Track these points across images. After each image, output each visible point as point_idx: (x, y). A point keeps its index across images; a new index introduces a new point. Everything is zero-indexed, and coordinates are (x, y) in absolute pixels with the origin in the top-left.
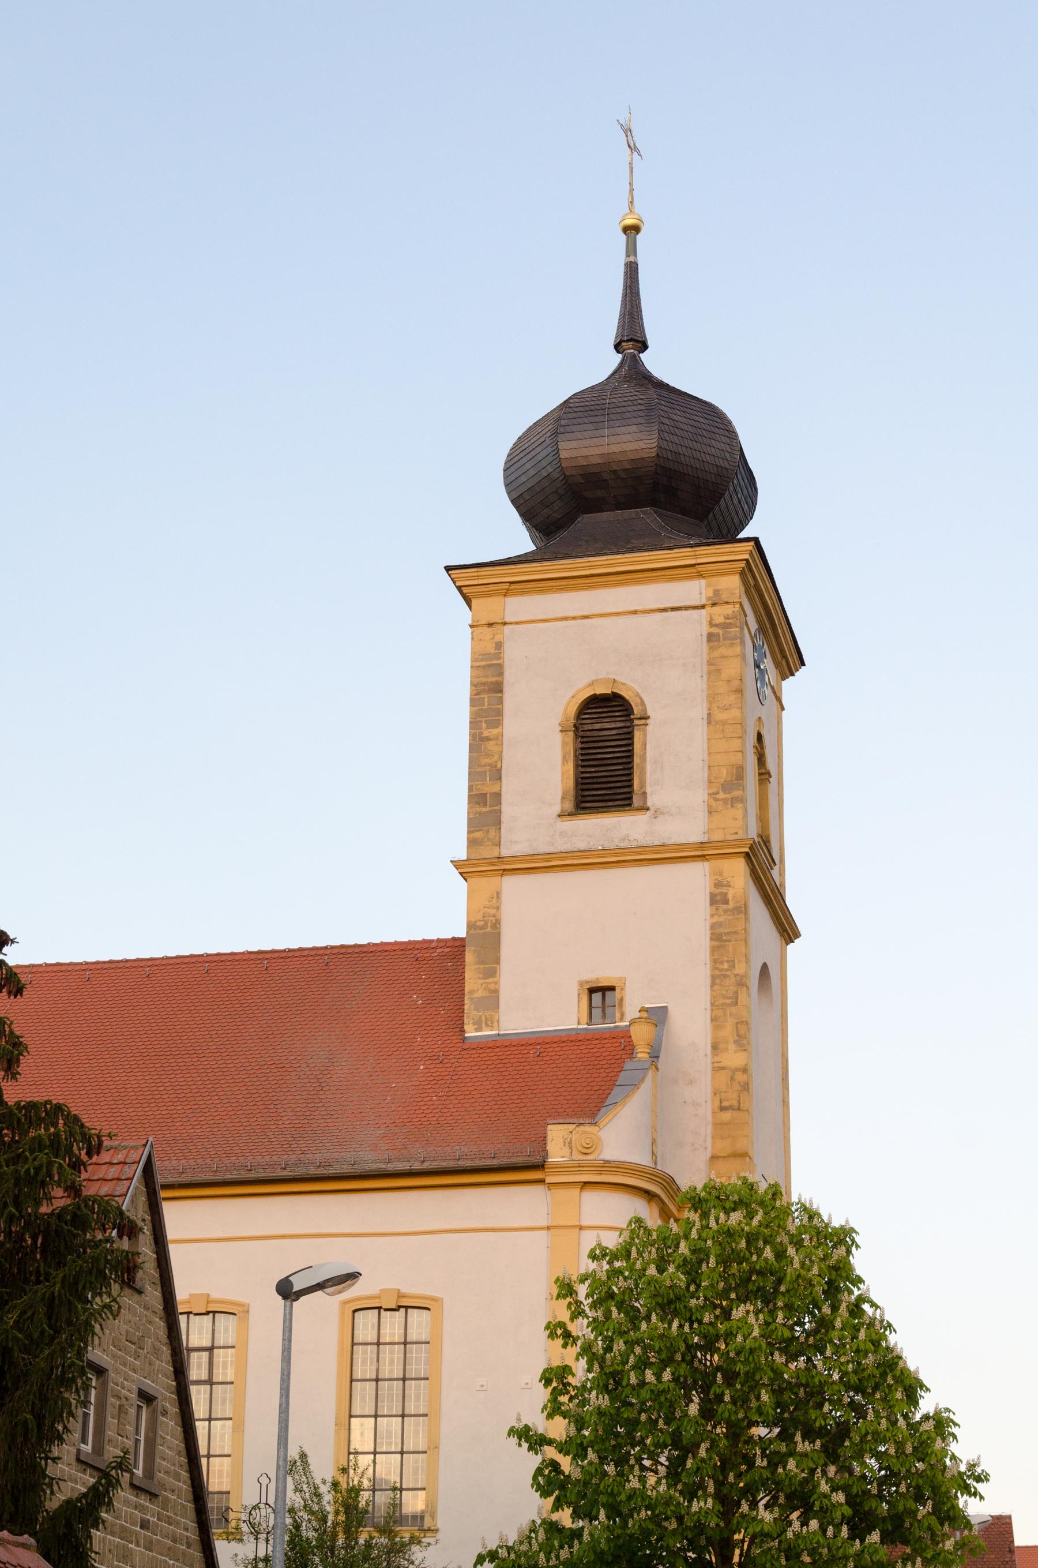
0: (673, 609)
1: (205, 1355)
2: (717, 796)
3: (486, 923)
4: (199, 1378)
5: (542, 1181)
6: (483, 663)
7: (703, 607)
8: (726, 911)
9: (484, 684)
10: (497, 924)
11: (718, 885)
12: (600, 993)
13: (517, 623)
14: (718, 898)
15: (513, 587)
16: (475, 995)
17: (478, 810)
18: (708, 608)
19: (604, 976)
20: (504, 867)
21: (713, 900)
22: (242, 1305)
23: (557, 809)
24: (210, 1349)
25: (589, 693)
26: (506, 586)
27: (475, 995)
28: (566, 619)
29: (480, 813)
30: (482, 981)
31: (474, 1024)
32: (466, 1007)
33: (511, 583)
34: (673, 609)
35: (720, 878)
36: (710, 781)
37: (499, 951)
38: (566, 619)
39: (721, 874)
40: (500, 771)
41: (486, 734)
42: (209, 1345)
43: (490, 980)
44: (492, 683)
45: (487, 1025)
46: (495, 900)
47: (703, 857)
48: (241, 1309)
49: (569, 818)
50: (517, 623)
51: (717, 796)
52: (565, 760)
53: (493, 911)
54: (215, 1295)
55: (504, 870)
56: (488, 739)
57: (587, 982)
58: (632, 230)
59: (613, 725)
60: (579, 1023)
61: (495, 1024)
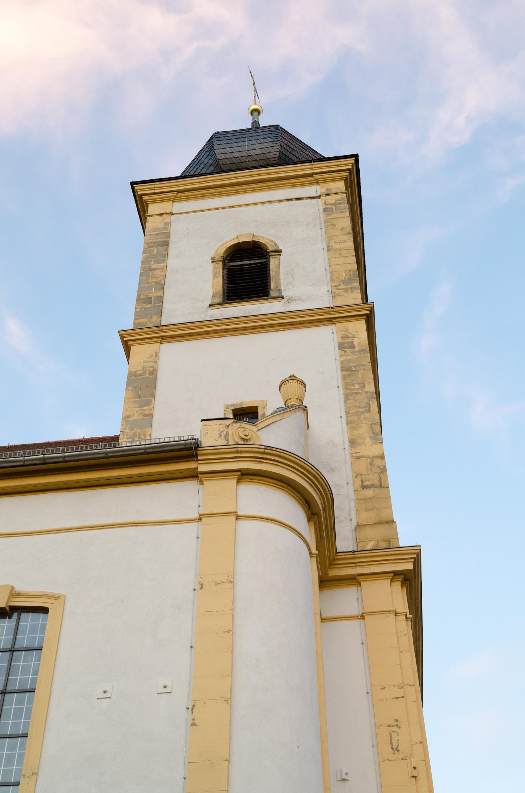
0: (297, 199)
5: (193, 475)
7: (319, 197)
14: (346, 345)
15: (179, 195)
16: (130, 419)
18: (323, 198)
20: (162, 334)
26: (175, 194)
33: (178, 192)
44: (160, 242)
47: (331, 321)
55: (163, 337)
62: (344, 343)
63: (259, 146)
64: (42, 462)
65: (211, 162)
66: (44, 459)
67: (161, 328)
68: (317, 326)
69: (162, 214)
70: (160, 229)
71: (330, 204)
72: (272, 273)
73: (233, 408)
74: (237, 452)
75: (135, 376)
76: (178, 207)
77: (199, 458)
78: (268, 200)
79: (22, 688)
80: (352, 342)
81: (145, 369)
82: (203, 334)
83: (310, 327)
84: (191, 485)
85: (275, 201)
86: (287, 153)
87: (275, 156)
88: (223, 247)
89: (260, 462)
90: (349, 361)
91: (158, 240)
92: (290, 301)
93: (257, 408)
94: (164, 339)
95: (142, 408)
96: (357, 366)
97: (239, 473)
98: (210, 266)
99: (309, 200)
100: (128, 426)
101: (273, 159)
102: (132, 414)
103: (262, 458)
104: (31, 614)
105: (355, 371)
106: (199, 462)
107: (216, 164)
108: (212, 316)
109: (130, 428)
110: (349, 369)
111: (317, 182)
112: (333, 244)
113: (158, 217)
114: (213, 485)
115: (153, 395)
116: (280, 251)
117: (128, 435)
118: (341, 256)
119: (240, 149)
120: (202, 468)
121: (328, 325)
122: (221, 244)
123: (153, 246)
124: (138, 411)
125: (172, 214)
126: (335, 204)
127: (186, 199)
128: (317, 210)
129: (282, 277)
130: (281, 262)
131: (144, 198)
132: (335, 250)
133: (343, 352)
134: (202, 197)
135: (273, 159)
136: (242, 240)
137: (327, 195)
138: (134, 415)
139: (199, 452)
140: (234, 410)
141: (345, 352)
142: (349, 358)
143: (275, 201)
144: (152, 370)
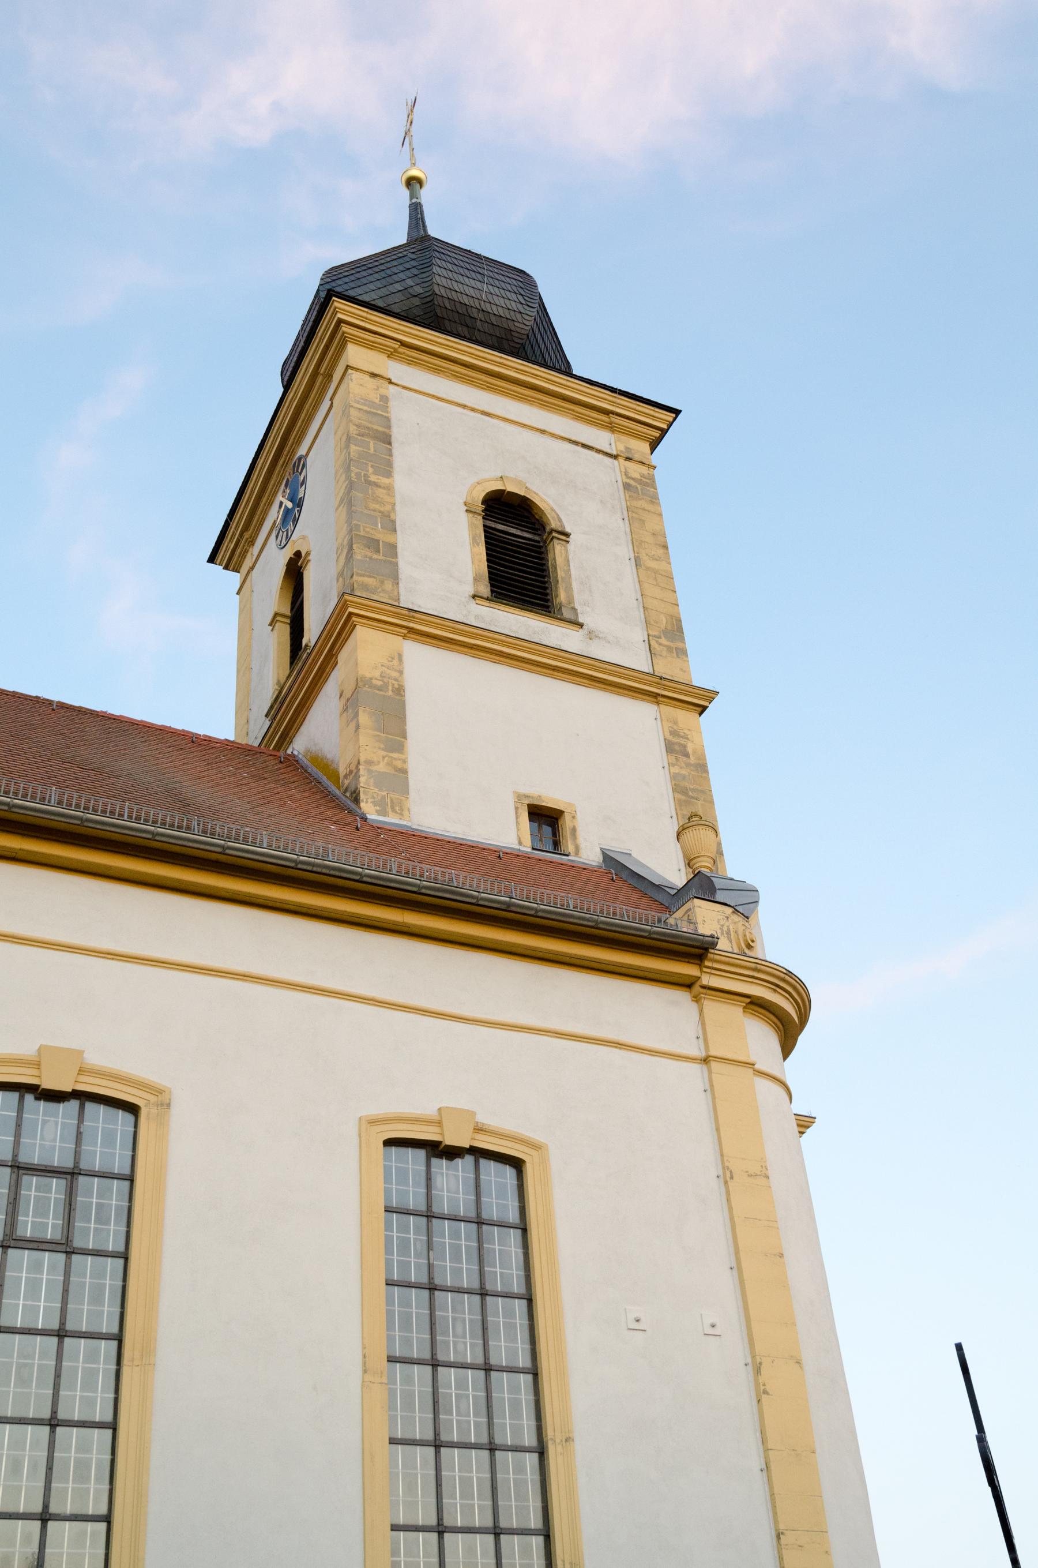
0: (584, 446)
1: (56, 1187)
2: (660, 641)
3: (386, 685)
4: (39, 1235)
5: (687, 984)
6: (365, 408)
7: (616, 457)
8: (688, 765)
9: (368, 428)
10: (400, 690)
11: (674, 733)
12: (545, 818)
13: (405, 388)
14: (677, 747)
15: (402, 350)
16: (374, 768)
17: (370, 554)
18: (621, 460)
19: (551, 797)
20: (411, 625)
21: (670, 747)
22: (157, 1091)
23: (470, 590)
24: (72, 1174)
25: (498, 486)
26: (396, 345)
27: (374, 768)
28: (464, 406)
29: (371, 558)
30: (384, 753)
31: (375, 804)
32: (362, 779)
33: (403, 344)
34: (584, 446)
35: (675, 727)
36: (647, 623)
37: (405, 724)
38: (464, 406)
39: (676, 723)
40: (394, 522)
41: (373, 478)
42: (69, 1164)
43: (395, 755)
44: (377, 430)
45: (394, 811)
46: (396, 662)
47: (655, 698)
48: (153, 1099)
49: (487, 603)
50: (405, 388)
51: (660, 641)
52: (474, 541)
53: (395, 674)
54: (94, 1059)
55: (411, 630)
56: (377, 485)
57: (527, 797)
58: (413, 183)
59: (519, 533)
60: (520, 843)
61: (406, 813)
62: (673, 744)
63: (501, 302)
64: (503, 907)
65: (418, 290)
66: (509, 904)
67: (412, 614)
68: (633, 698)
69: (374, 375)
70: (372, 404)
71: (633, 479)
72: (561, 573)
73: (527, 802)
74: (755, 970)
75: (370, 687)
76: (396, 370)
77: (707, 963)
78: (543, 428)
79: (106, 1169)
80: (685, 747)
81: (385, 680)
82: (472, 648)
83: (624, 695)
84: (681, 996)
85: (553, 435)
86: (537, 332)
87: (523, 332)
88: (479, 488)
89: (775, 990)
90: (684, 777)
91: (375, 427)
92: (591, 635)
93: (561, 813)
94: (412, 633)
95: (391, 755)
96: (693, 790)
97: (748, 1000)
98: (464, 518)
99: (601, 456)
100: (372, 781)
101: (517, 335)
102: (375, 759)
103: (778, 986)
104: (492, 1162)
105: (693, 797)
106: (705, 970)
107: (428, 299)
108: (477, 617)
109: (376, 785)
110: (684, 791)
111: (611, 428)
112: (644, 557)
113: (367, 378)
114: (716, 1009)
115: (404, 735)
116: (567, 535)
117: (373, 797)
118: (657, 585)
119: (471, 292)
120: (706, 980)
121: (652, 702)
122: (476, 480)
123: (368, 435)
124: (384, 758)
125: (390, 382)
126: (640, 482)
127: (411, 362)
128: (614, 481)
129: (575, 585)
130: (571, 556)
131: (344, 328)
132: (648, 569)
133: (672, 759)
134: (437, 370)
135: (517, 335)
136: (511, 488)
137: (628, 459)
138: (379, 762)
139: (710, 956)
140: (529, 805)
141: (677, 759)
142: (683, 772)
143: (553, 435)
144: (396, 686)
